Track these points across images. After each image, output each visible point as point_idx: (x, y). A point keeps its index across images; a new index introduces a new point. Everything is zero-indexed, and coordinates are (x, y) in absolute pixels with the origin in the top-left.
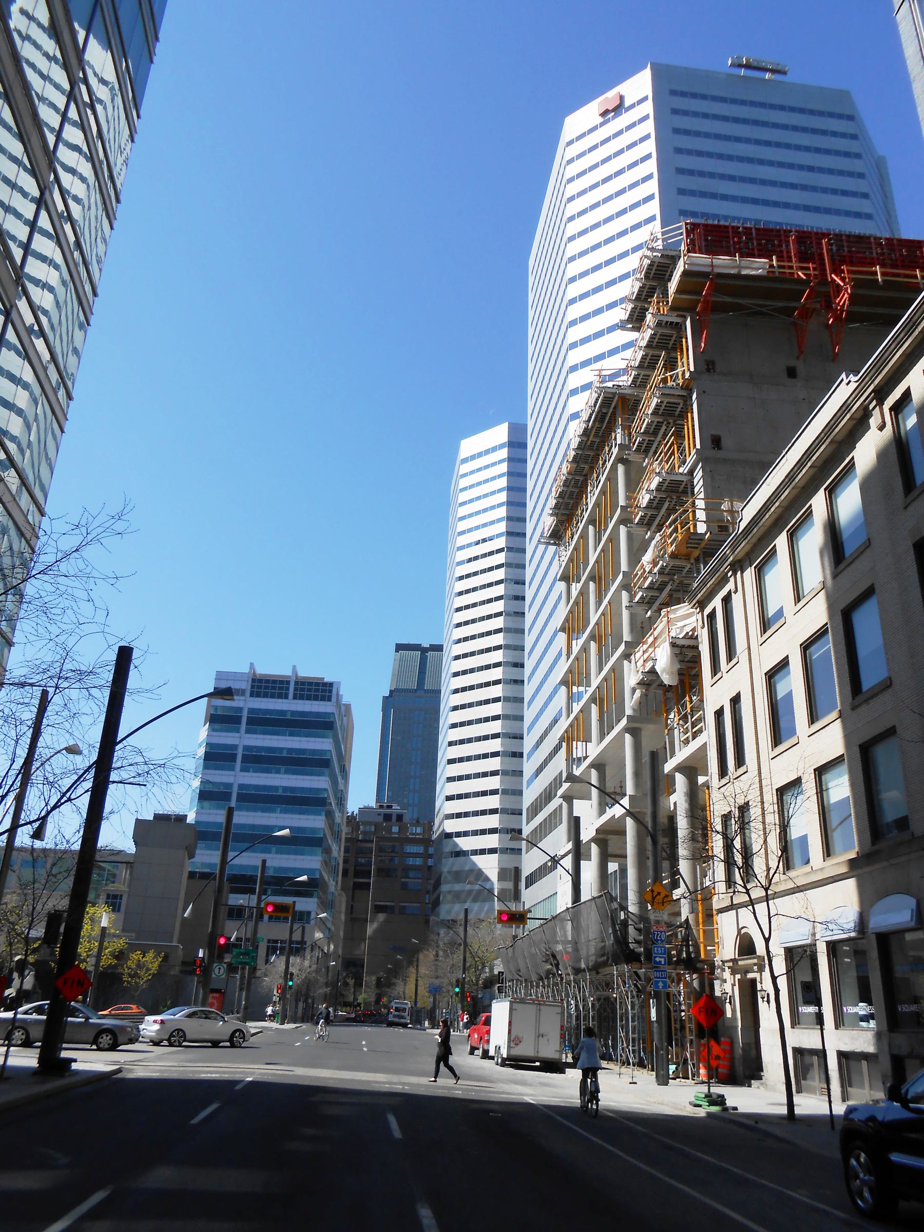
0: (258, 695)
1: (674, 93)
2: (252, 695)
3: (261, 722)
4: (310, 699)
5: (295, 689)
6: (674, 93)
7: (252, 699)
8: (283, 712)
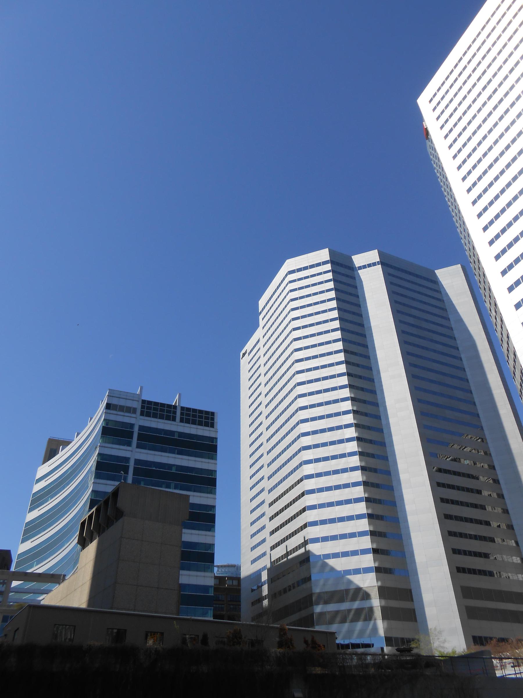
0: (148, 415)
1: (440, 470)
2: (142, 414)
3: (150, 439)
4: (163, 418)
5: (182, 414)
6: (440, 470)
7: (142, 417)
8: (172, 433)
